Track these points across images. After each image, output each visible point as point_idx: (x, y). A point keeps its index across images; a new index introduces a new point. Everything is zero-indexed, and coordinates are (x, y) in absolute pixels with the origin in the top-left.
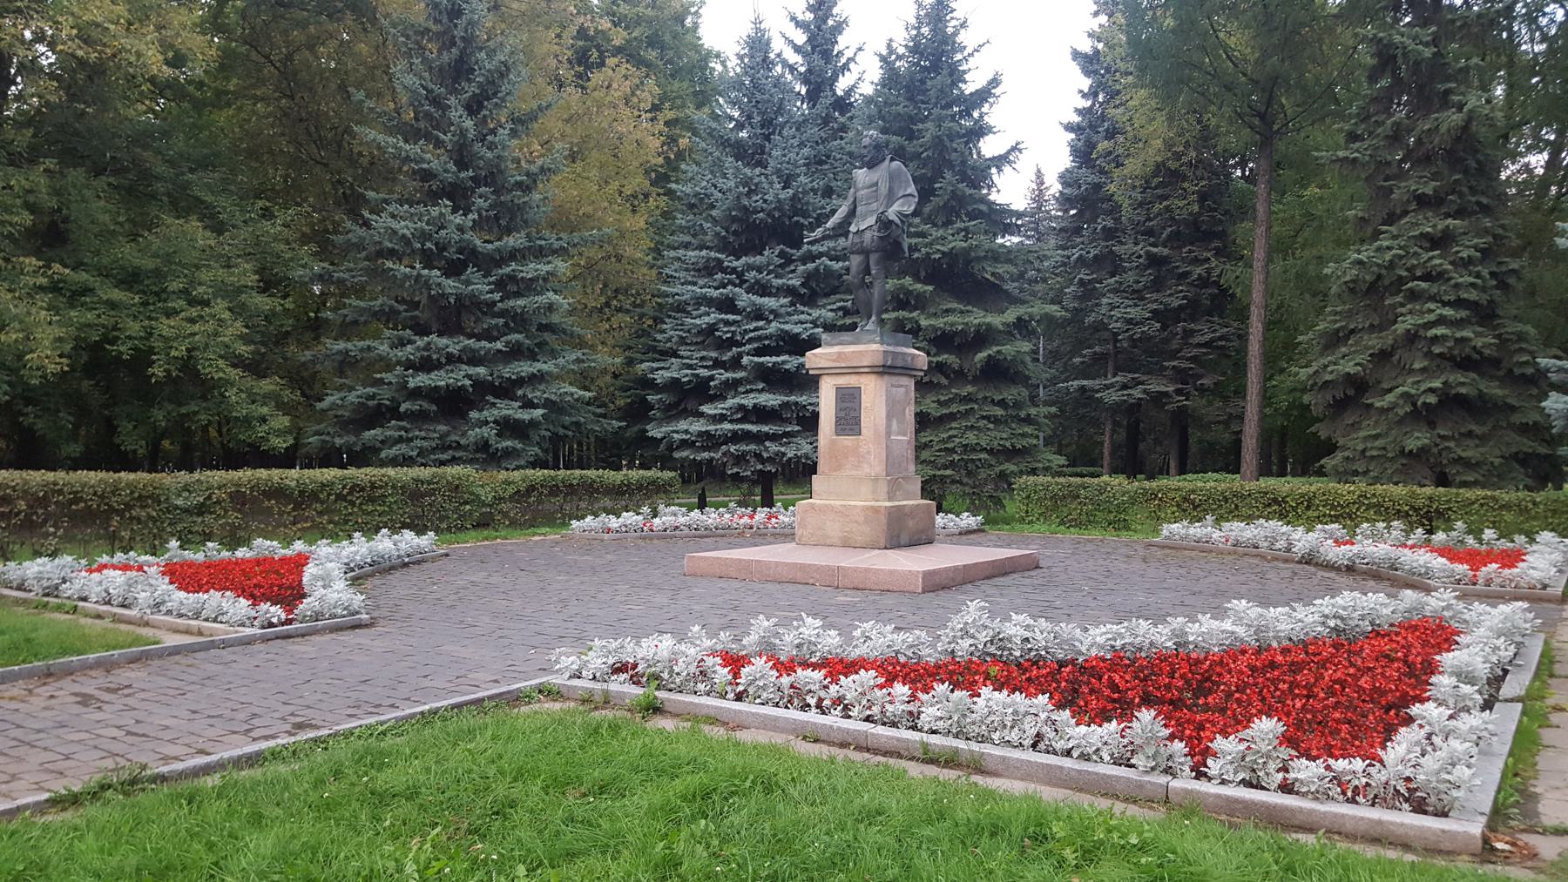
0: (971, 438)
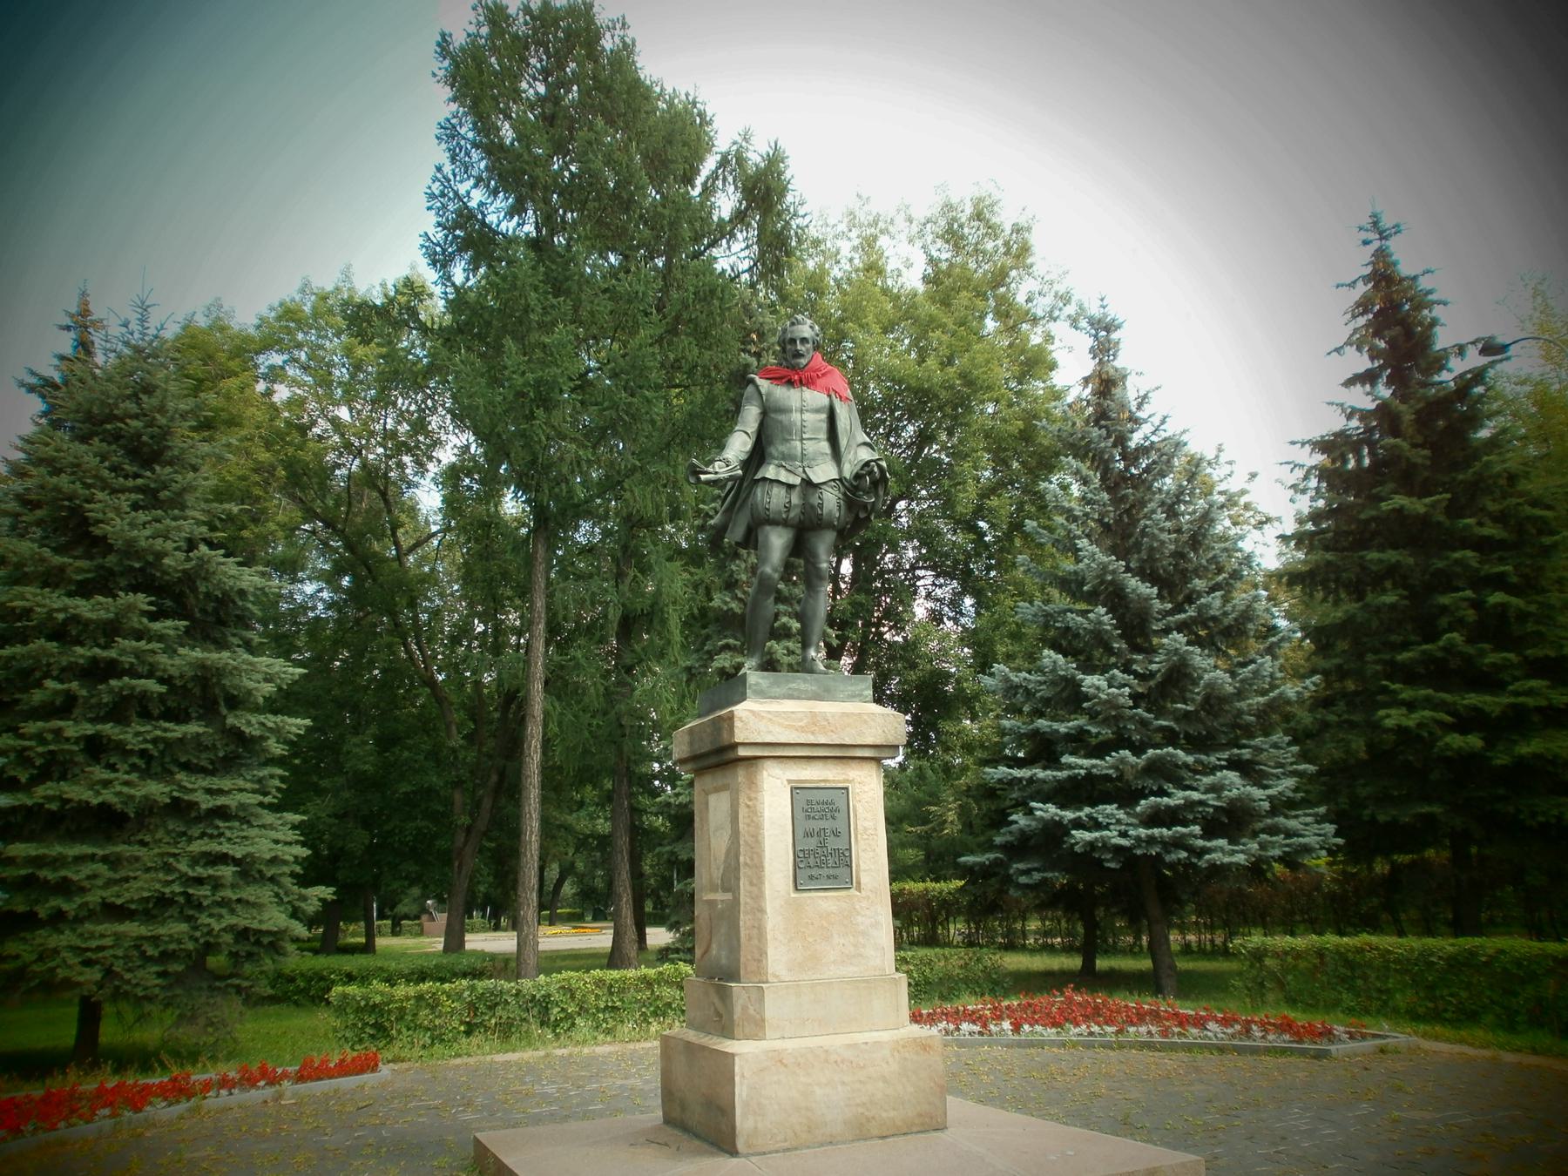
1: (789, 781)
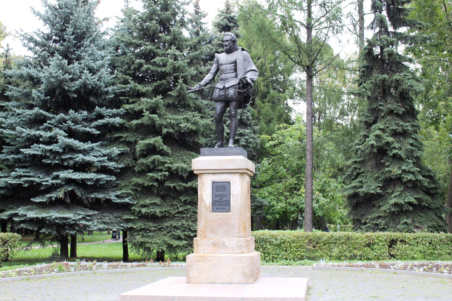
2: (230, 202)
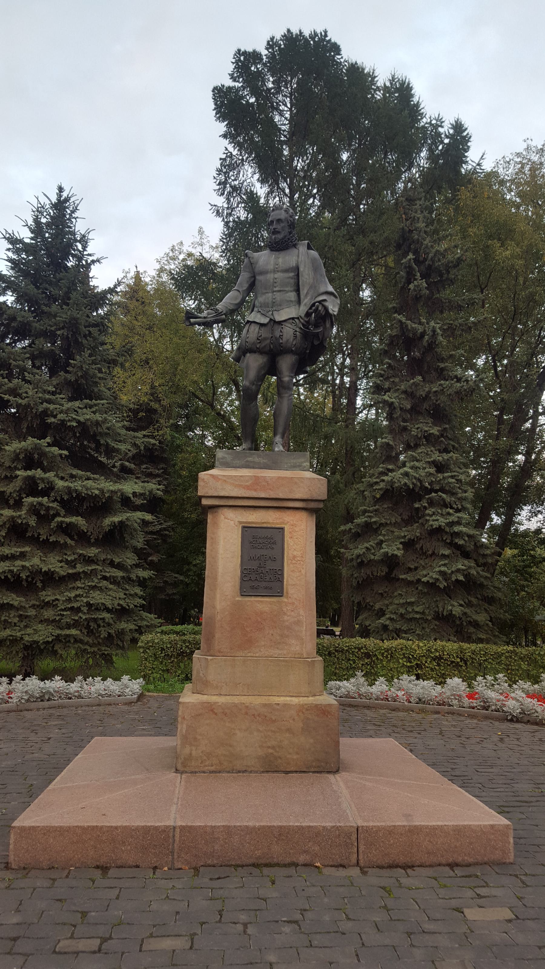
0: (97, 597)
1: (240, 523)
2: (282, 575)
